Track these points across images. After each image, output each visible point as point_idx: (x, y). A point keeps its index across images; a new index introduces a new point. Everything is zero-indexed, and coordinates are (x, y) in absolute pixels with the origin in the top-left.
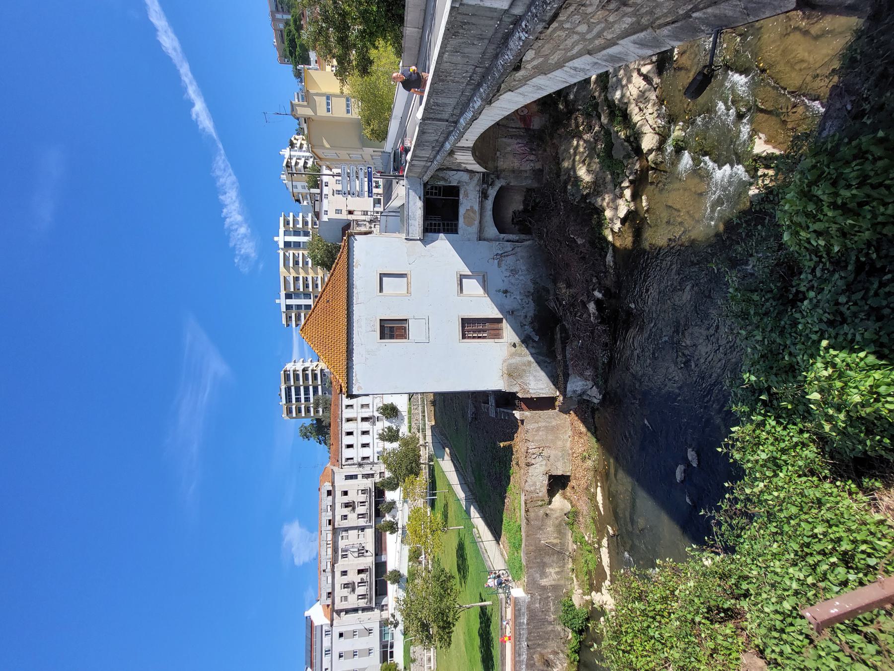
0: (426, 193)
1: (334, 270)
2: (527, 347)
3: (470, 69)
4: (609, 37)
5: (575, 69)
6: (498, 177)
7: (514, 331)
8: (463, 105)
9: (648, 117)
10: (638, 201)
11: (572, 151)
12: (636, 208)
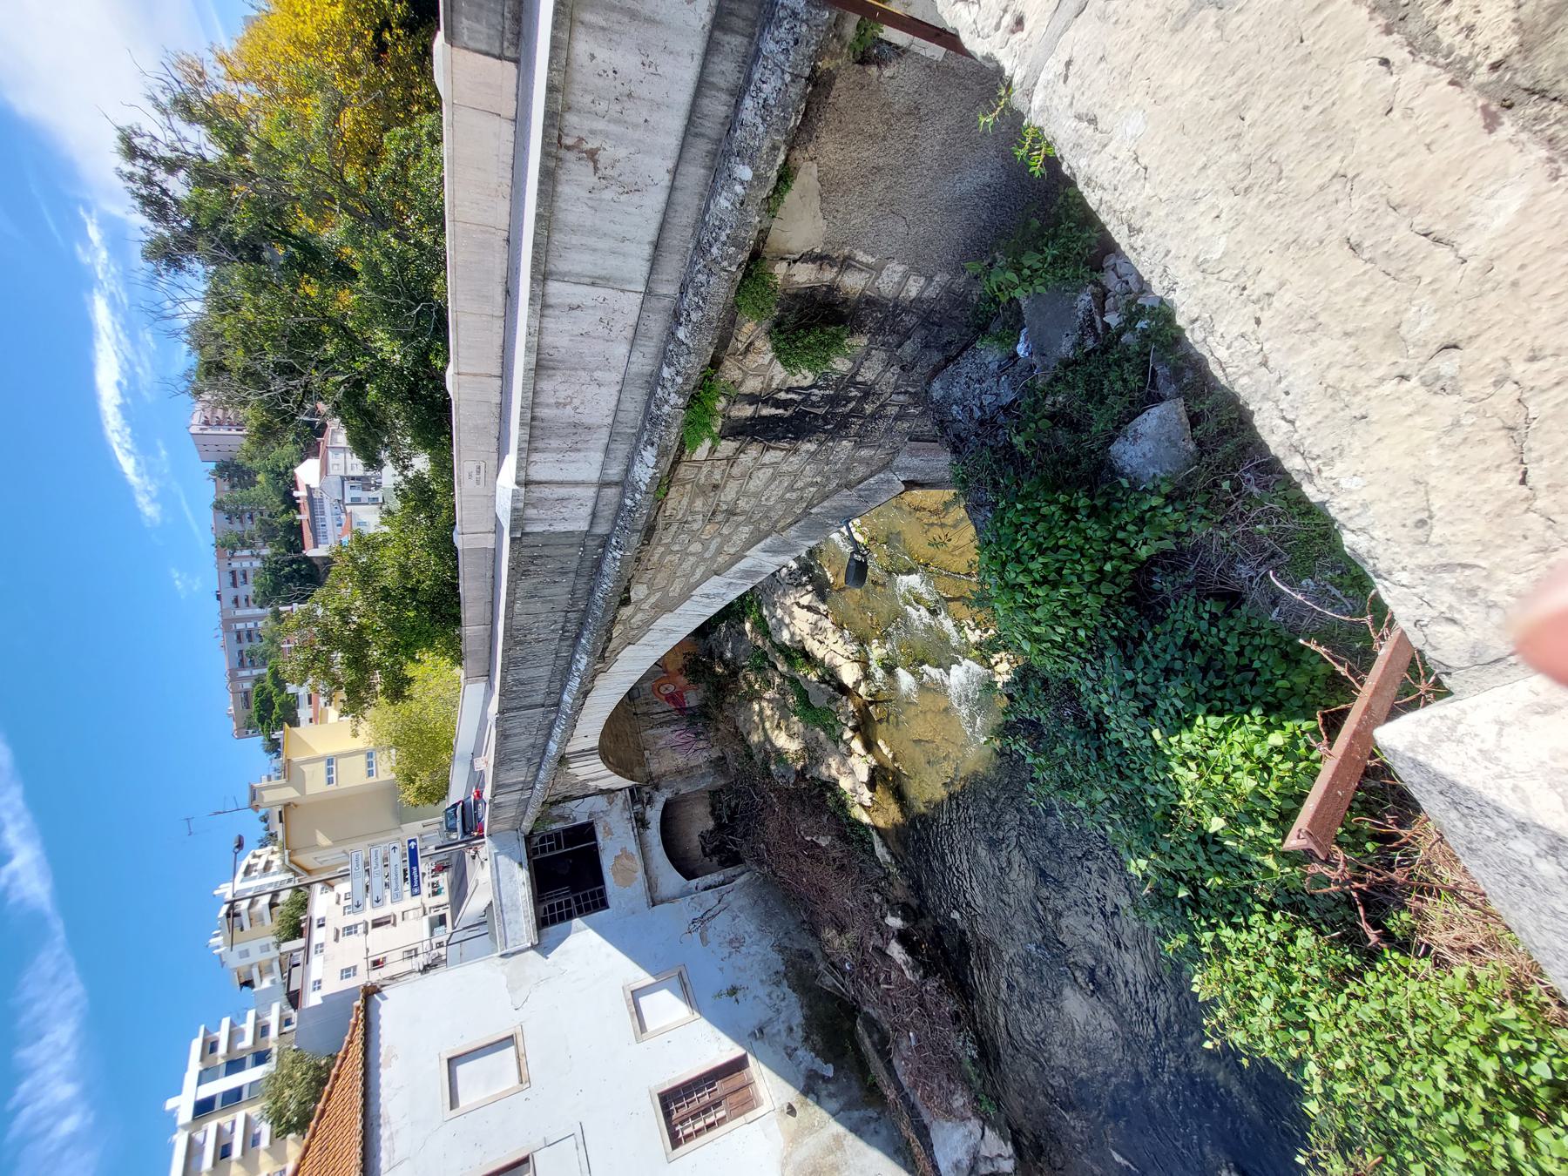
0: (531, 853)
1: (328, 1100)
2: (818, 1103)
3: (559, 617)
4: (732, 551)
5: (708, 596)
6: (657, 788)
7: (778, 1073)
8: (562, 673)
9: (834, 647)
10: (877, 750)
11: (756, 718)
12: (878, 761)
